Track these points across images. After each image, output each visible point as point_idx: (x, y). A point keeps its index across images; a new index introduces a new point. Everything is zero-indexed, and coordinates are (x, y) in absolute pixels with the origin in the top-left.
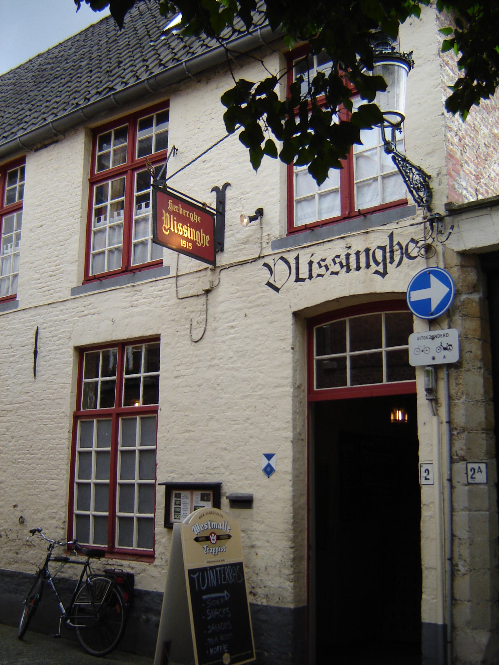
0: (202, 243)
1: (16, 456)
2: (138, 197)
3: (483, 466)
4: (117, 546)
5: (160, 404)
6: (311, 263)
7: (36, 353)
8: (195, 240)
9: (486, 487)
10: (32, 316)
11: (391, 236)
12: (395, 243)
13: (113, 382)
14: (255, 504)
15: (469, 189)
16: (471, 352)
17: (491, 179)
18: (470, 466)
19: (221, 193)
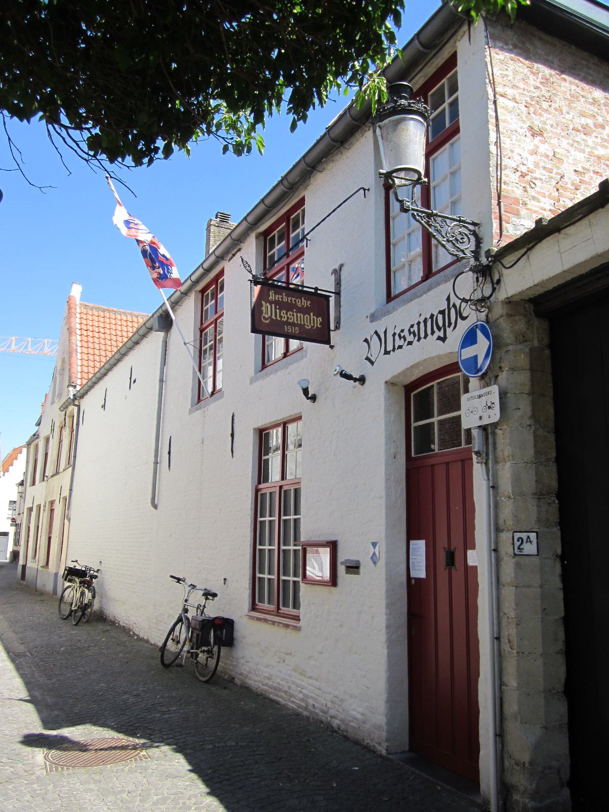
0: (312, 325)
3: (533, 536)
8: (303, 323)
9: (536, 560)
12: (451, 304)
16: (519, 409)
18: (517, 535)
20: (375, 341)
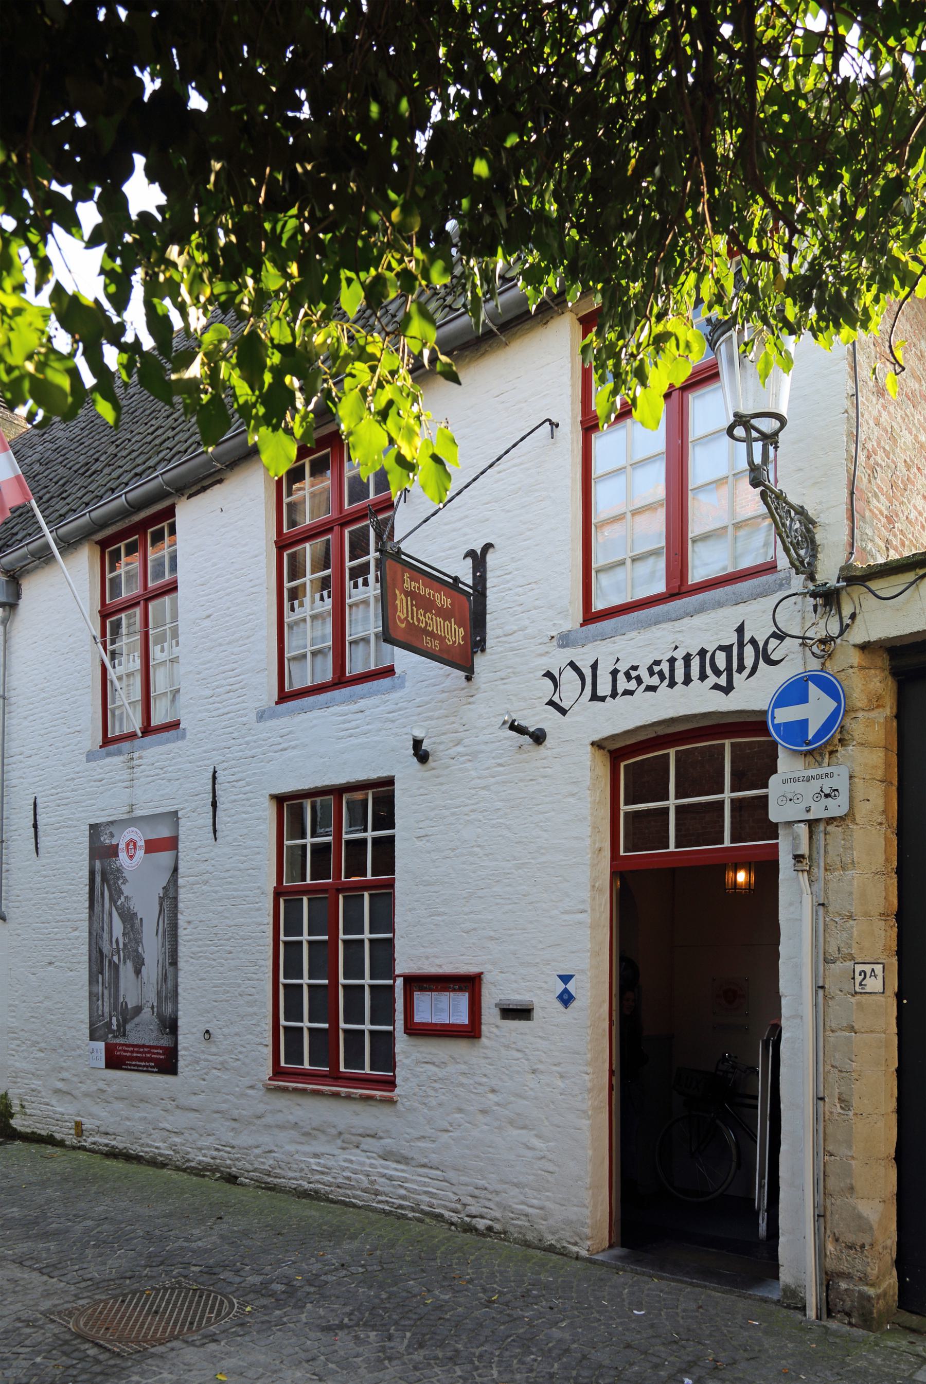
1: (195, 949)
2: (351, 569)
3: (878, 968)
4: (342, 1069)
5: (397, 876)
6: (615, 673)
7: (214, 804)
10: (205, 752)
11: (740, 630)
13: (327, 845)
14: (536, 1014)
15: (877, 540)
17: (910, 522)
18: (859, 968)
19: (479, 559)
20: (569, 678)
